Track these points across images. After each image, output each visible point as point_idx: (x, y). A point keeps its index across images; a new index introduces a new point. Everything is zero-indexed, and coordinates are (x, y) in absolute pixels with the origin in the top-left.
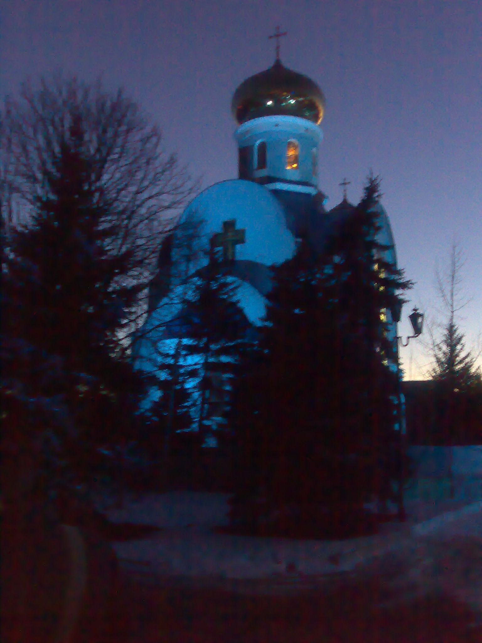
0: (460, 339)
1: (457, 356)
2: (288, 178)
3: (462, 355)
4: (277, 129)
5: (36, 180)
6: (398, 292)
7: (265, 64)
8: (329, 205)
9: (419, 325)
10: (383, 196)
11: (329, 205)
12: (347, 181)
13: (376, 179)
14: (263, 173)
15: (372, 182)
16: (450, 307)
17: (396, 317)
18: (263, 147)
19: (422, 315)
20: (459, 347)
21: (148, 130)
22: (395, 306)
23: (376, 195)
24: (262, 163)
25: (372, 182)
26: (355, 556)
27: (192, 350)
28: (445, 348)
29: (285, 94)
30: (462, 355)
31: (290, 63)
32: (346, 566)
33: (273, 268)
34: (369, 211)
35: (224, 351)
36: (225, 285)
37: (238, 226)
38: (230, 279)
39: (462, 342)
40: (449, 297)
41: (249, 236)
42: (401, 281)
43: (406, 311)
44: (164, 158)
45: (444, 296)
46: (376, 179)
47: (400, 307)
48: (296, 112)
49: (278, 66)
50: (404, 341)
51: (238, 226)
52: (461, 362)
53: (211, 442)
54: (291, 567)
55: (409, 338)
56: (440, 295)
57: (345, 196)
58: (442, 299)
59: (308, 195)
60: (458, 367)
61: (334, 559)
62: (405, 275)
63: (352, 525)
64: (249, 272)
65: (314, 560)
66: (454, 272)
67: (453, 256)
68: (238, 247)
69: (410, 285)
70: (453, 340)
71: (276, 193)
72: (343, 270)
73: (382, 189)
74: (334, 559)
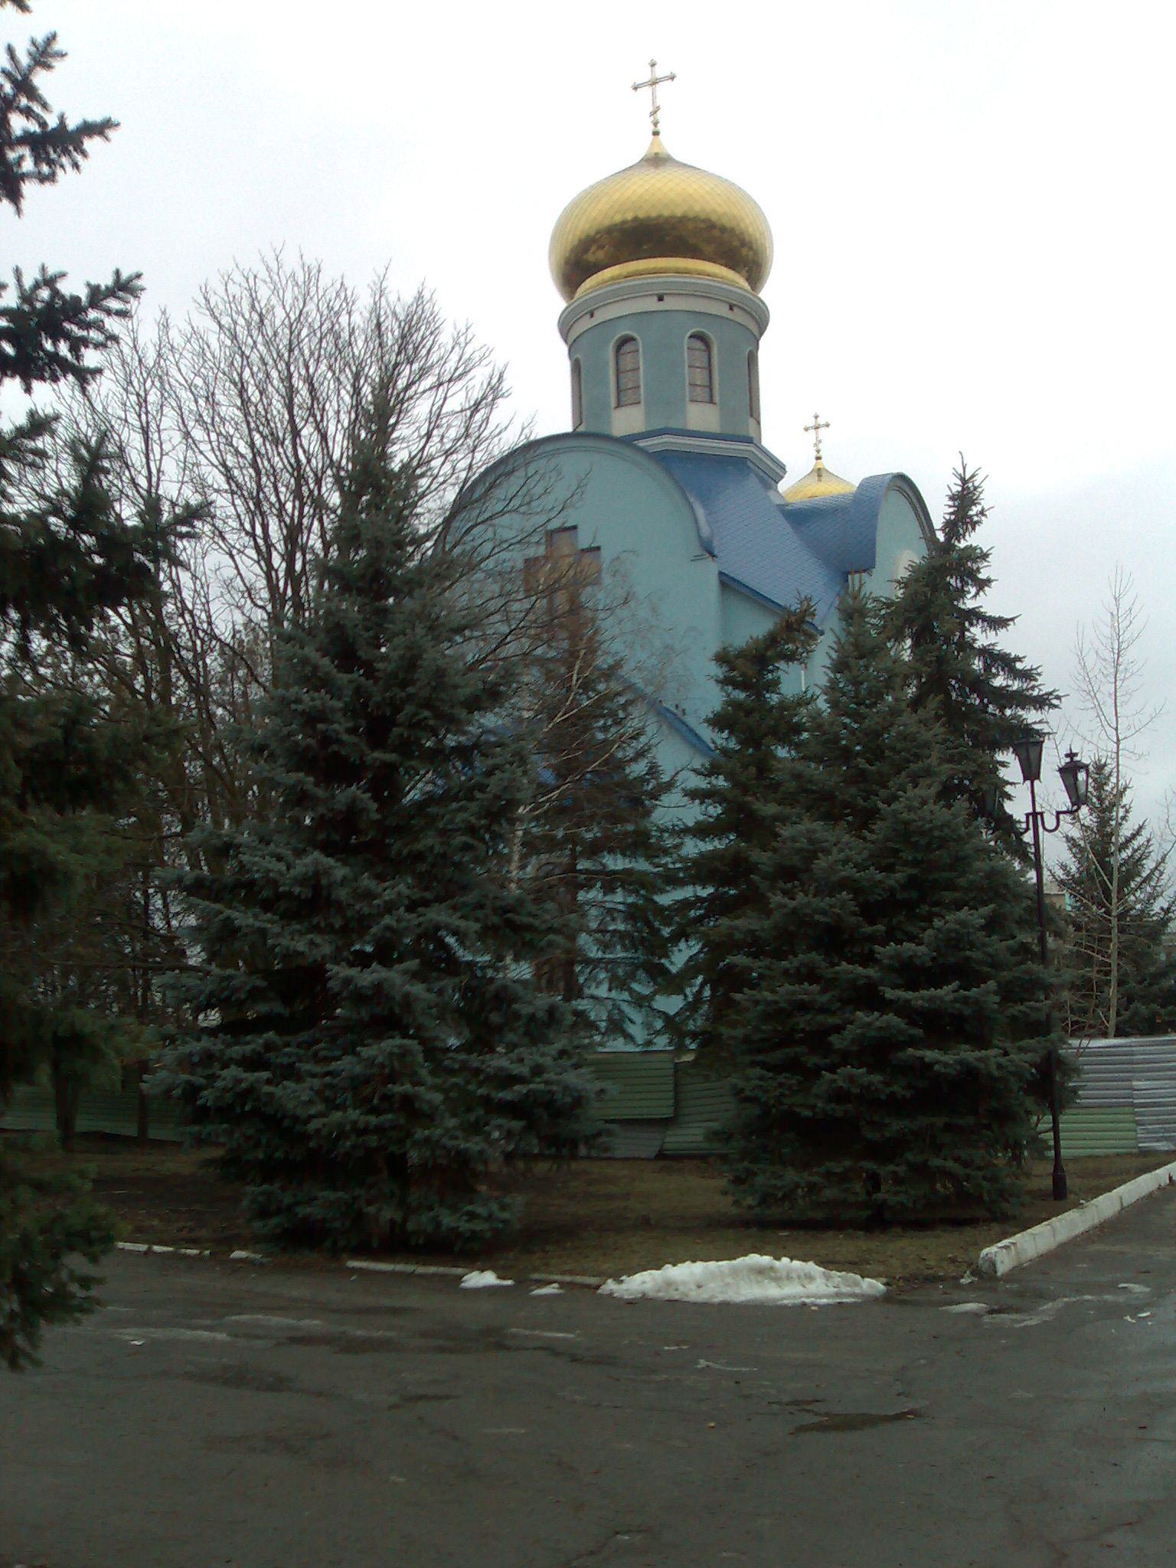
3: (1126, 830)
17: (1031, 772)
21: (478, 381)
22: (1028, 744)
23: (975, 510)
30: (1126, 830)
39: (1125, 801)
40: (1109, 710)
43: (1051, 759)
50: (1050, 822)
55: (1058, 813)
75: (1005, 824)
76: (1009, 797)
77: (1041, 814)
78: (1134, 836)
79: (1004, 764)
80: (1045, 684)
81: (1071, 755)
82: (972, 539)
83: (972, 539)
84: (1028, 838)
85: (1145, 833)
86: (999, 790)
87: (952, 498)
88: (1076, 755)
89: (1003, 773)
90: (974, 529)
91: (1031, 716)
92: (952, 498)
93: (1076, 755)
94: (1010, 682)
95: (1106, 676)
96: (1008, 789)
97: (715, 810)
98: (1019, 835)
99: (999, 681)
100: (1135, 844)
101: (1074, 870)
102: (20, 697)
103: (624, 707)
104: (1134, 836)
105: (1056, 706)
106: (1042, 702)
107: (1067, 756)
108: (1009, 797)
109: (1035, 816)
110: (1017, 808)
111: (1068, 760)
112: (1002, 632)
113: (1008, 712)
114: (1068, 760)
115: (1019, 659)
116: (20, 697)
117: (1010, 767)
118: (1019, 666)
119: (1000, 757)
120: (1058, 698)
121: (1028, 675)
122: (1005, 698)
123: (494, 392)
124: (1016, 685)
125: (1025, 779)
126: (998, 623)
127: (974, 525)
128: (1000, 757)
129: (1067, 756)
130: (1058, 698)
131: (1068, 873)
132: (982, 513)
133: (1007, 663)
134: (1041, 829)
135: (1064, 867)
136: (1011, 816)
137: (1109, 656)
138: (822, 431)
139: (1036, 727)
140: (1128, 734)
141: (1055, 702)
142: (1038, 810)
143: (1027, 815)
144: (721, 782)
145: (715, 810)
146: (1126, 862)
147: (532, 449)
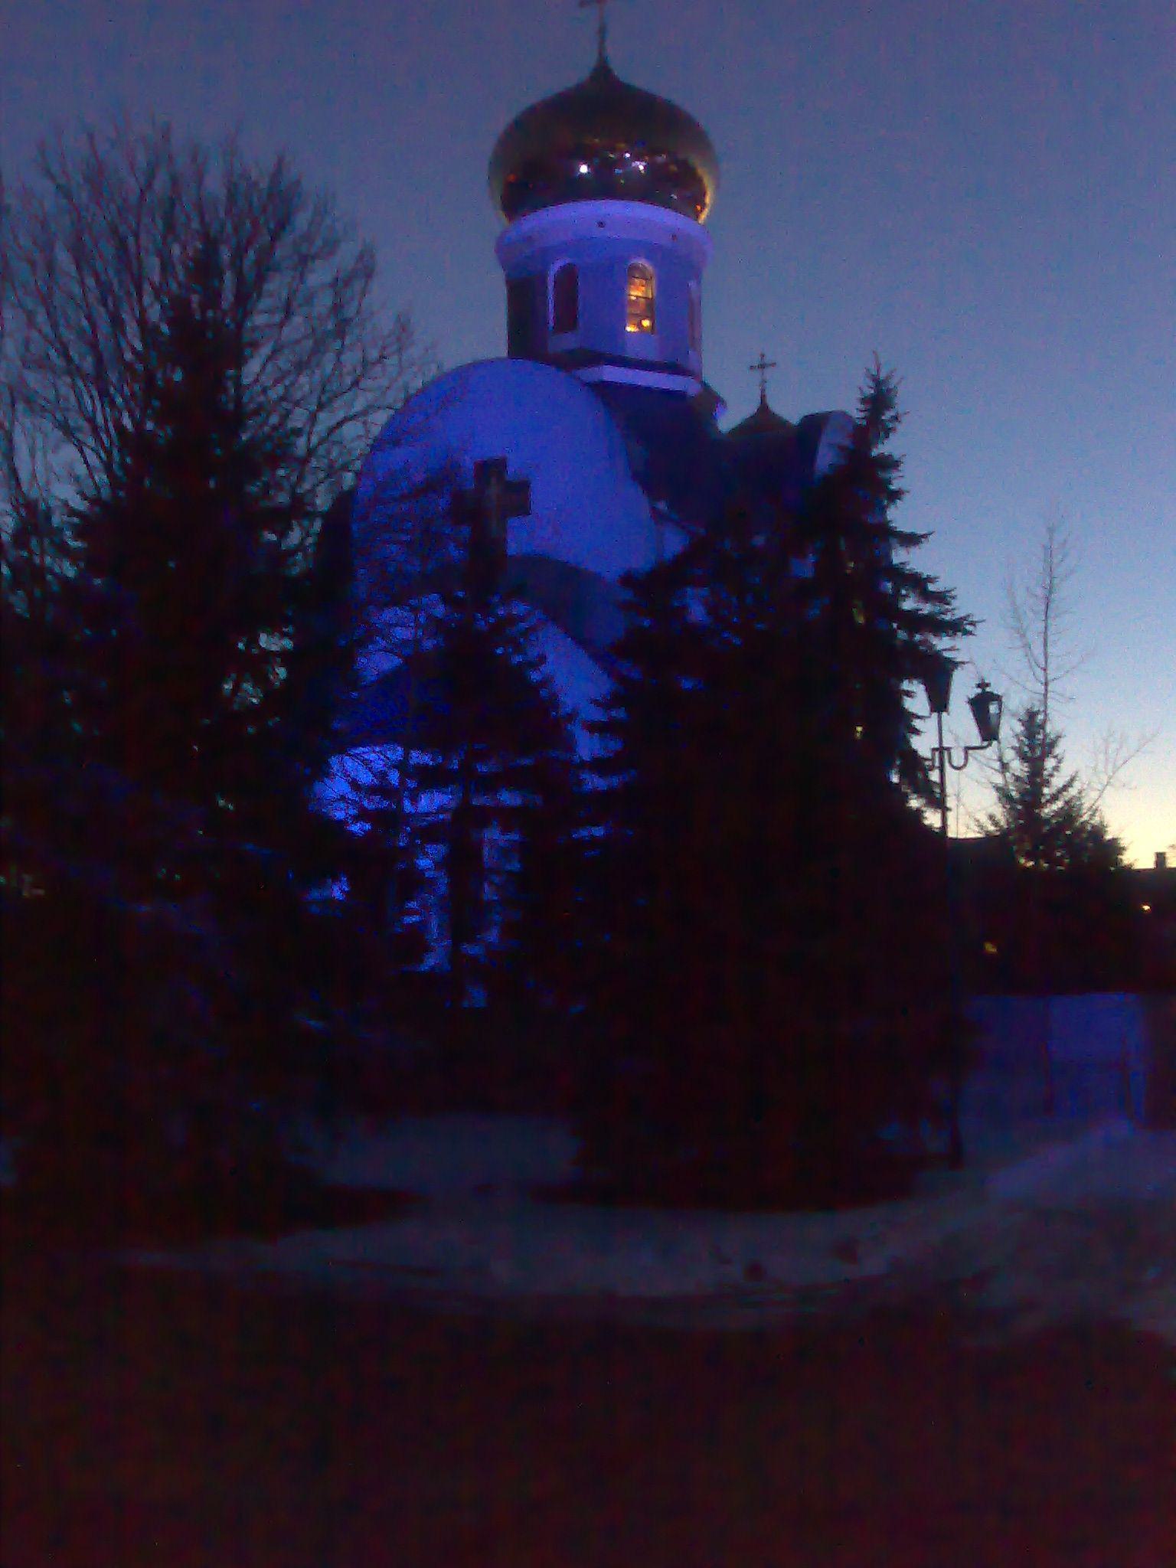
0: (1053, 744)
1: (1047, 783)
2: (630, 354)
3: (1058, 782)
4: (598, 232)
5: (53, 369)
6: (941, 643)
7: (570, 72)
8: (727, 422)
9: (993, 720)
10: (904, 419)
11: (727, 422)
12: (767, 360)
13: (888, 377)
14: (568, 342)
15: (878, 383)
16: (1040, 673)
17: (939, 703)
18: (569, 275)
19: (997, 698)
20: (1050, 763)
21: (346, 257)
22: (937, 676)
23: (887, 415)
24: (568, 317)
25: (878, 383)
26: (885, 1243)
27: (430, 779)
28: (1018, 767)
29: (622, 145)
30: (1058, 782)
31: (637, 72)
32: (873, 1265)
33: (628, 579)
34: (875, 452)
35: (510, 778)
36: (512, 620)
37: (512, 472)
38: (519, 609)
39: (1057, 751)
40: (1038, 651)
41: (540, 499)
42: (948, 617)
43: (962, 688)
44: (385, 323)
45: (1027, 646)
46: (888, 377)
47: (948, 676)
48: (648, 191)
49: (602, 71)
50: (958, 758)
51: (512, 472)
52: (1054, 798)
53: (477, 997)
54: (755, 1271)
55: (967, 749)
56: (1019, 643)
57: (763, 397)
58: (1021, 652)
59: (680, 395)
60: (1048, 811)
61: (847, 1251)
62: (955, 603)
63: (872, 1178)
64: (562, 591)
65: (804, 1256)
66: (1050, 590)
67: (1049, 552)
68: (513, 522)
69: (969, 628)
70: (1037, 746)
71: (604, 390)
72: (795, 585)
73: (903, 400)
74: (847, 1251)
75: (913, 764)
76: (917, 732)
77: (948, 749)
78: (1065, 788)
79: (909, 694)
80: (960, 608)
81: (982, 685)
82: (882, 448)
83: (882, 448)
84: (934, 776)
85: (1077, 785)
86: (905, 722)
87: (864, 401)
88: (988, 685)
89: (909, 704)
90: (887, 437)
91: (941, 643)
92: (864, 401)
93: (988, 685)
94: (921, 606)
95: (1035, 613)
96: (917, 723)
97: (615, 745)
98: (926, 771)
99: (908, 605)
100: (1066, 796)
101: (1003, 823)
102: (1022, 861)
103: (526, 633)
104: (1065, 788)
105: (970, 633)
106: (956, 627)
107: (979, 686)
108: (917, 732)
109: (941, 750)
110: (923, 744)
111: (979, 691)
112: (915, 551)
113: (918, 637)
114: (979, 691)
115: (930, 580)
116: (1022, 861)
117: (916, 699)
118: (931, 587)
119: (906, 685)
120: (972, 624)
121: (941, 598)
122: (916, 622)
123: (365, 269)
124: (927, 609)
125: (932, 710)
126: (911, 540)
127: (888, 432)
128: (906, 685)
129: (979, 686)
130: (972, 624)
131: (996, 824)
132: (896, 418)
133: (919, 583)
134: (947, 764)
135: (991, 817)
136: (915, 752)
137: (1040, 592)
138: (768, 371)
139: (946, 654)
140: (1059, 674)
141: (969, 628)
142: (945, 745)
143: (934, 750)
144: (619, 714)
145: (615, 745)
146: (1057, 814)
147: (464, 375)
